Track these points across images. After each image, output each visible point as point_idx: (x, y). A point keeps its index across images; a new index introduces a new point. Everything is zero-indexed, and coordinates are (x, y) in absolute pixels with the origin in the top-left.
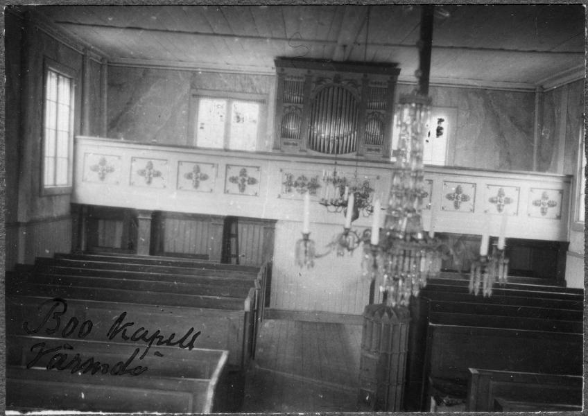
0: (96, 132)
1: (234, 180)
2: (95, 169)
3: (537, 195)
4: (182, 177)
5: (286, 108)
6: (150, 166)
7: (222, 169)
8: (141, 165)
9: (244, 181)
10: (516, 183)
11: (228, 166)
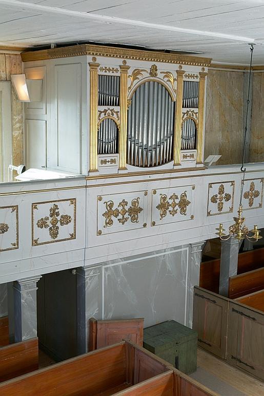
5: (101, 112)
9: (54, 223)
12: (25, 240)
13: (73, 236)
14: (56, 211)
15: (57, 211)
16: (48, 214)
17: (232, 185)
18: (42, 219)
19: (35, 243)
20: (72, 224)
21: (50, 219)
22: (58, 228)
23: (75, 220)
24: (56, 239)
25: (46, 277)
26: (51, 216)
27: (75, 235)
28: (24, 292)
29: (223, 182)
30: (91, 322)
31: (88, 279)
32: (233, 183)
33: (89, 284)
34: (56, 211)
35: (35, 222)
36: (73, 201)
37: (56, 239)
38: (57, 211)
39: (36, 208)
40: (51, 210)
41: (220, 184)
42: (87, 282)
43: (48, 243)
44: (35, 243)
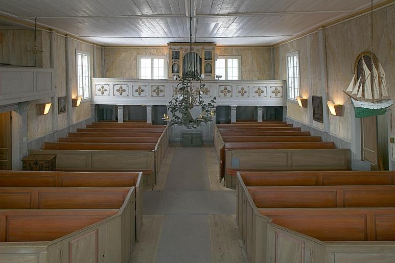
0: (103, 76)
1: (154, 91)
2: (99, 90)
3: (273, 89)
4: (134, 91)
6: (121, 87)
7: (130, 86)
8: (117, 87)
10: (248, 85)
12: (268, 95)
36: (232, 86)
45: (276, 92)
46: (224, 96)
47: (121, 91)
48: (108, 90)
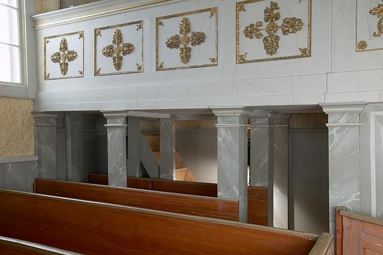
1: (251, 31)
7: (149, 25)
9: (272, 29)
11: (159, 22)
13: (306, 53)
14: (274, 12)
15: (275, 12)
16: (261, 17)
17: (81, 36)
18: (252, 25)
19: (241, 60)
20: (304, 31)
21: (265, 24)
22: (277, 38)
23: (310, 25)
24: (274, 56)
25: (325, 117)
26: (267, 21)
27: (310, 52)
28: (339, 142)
29: (65, 35)
30: (335, 209)
31: (335, 129)
32: (139, 24)
33: (336, 140)
34: (274, 12)
35: (242, 29)
37: (274, 56)
38: (275, 12)
39: (161, 24)
40: (266, 11)
41: (181, 18)
42: (332, 135)
43: (262, 60)
44: (241, 60)
45: (65, 57)
46: (264, 55)
47: (119, 51)
48: (49, 60)
